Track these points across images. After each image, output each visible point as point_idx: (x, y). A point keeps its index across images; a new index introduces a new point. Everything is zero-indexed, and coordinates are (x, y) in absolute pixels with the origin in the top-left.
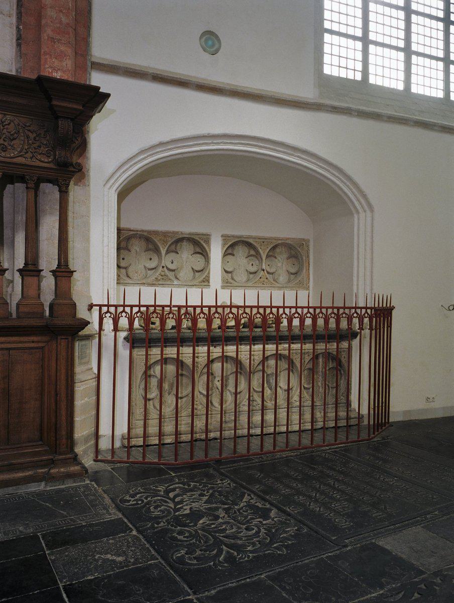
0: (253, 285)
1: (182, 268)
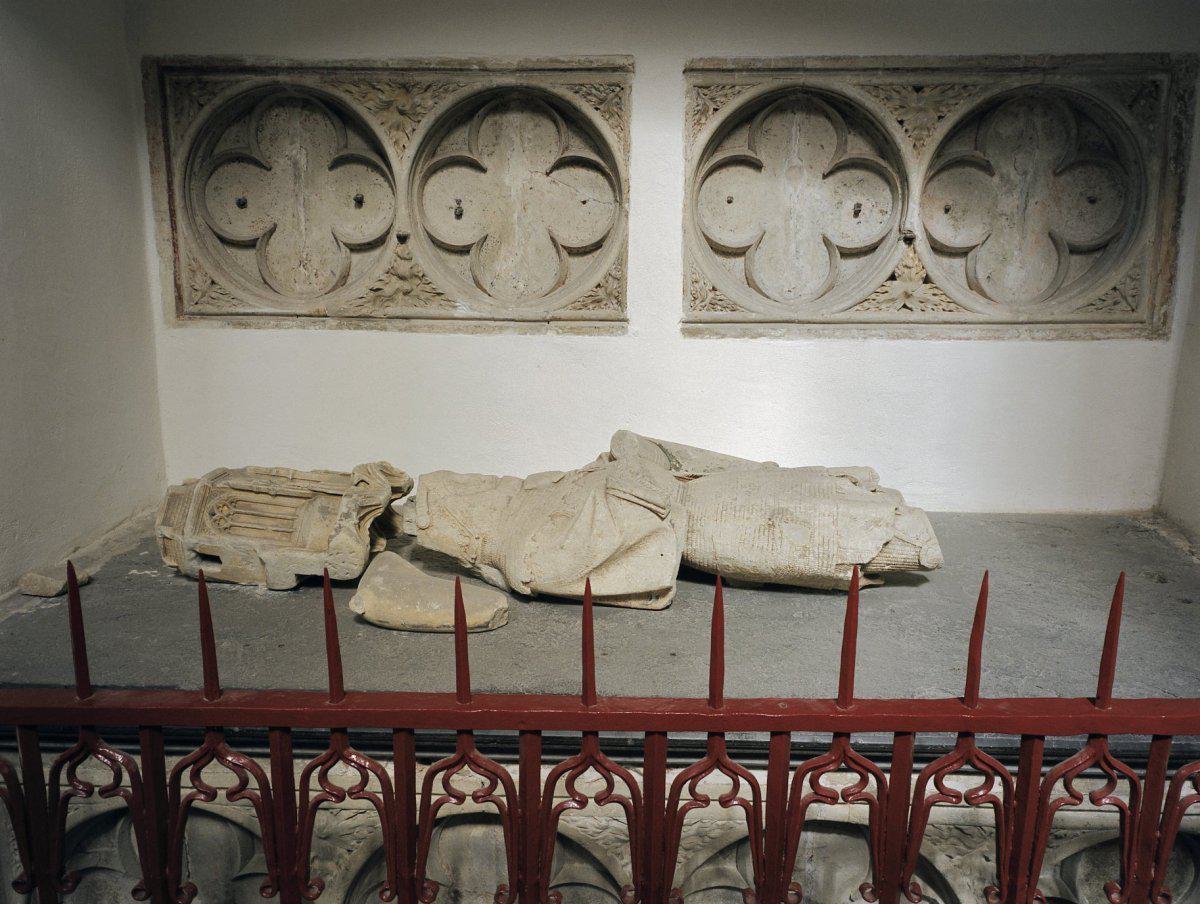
0: (852, 315)
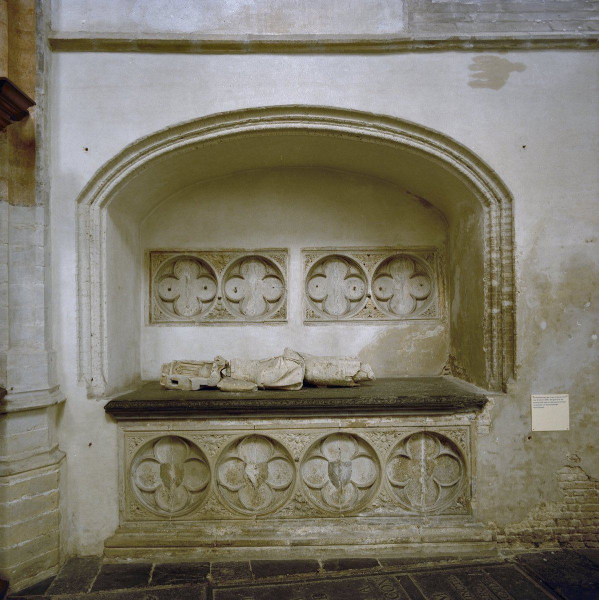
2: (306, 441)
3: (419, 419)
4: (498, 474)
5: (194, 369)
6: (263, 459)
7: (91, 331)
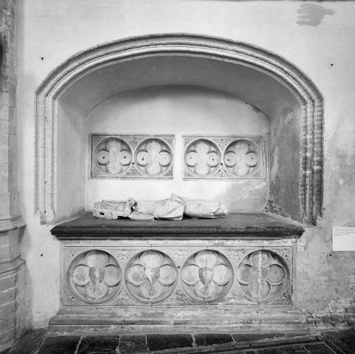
0: (211, 177)
1: (151, 164)
2: (185, 254)
3: (259, 241)
4: (310, 278)
5: (115, 206)
6: (157, 265)
7: (45, 181)
